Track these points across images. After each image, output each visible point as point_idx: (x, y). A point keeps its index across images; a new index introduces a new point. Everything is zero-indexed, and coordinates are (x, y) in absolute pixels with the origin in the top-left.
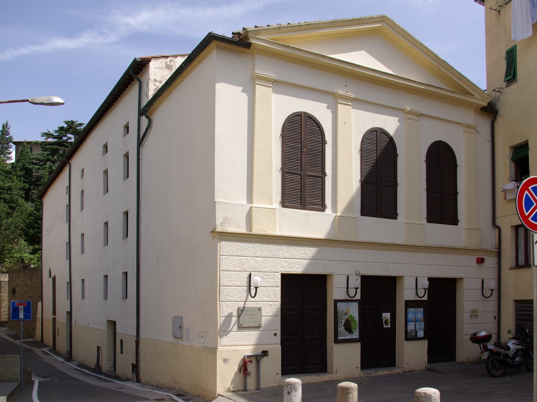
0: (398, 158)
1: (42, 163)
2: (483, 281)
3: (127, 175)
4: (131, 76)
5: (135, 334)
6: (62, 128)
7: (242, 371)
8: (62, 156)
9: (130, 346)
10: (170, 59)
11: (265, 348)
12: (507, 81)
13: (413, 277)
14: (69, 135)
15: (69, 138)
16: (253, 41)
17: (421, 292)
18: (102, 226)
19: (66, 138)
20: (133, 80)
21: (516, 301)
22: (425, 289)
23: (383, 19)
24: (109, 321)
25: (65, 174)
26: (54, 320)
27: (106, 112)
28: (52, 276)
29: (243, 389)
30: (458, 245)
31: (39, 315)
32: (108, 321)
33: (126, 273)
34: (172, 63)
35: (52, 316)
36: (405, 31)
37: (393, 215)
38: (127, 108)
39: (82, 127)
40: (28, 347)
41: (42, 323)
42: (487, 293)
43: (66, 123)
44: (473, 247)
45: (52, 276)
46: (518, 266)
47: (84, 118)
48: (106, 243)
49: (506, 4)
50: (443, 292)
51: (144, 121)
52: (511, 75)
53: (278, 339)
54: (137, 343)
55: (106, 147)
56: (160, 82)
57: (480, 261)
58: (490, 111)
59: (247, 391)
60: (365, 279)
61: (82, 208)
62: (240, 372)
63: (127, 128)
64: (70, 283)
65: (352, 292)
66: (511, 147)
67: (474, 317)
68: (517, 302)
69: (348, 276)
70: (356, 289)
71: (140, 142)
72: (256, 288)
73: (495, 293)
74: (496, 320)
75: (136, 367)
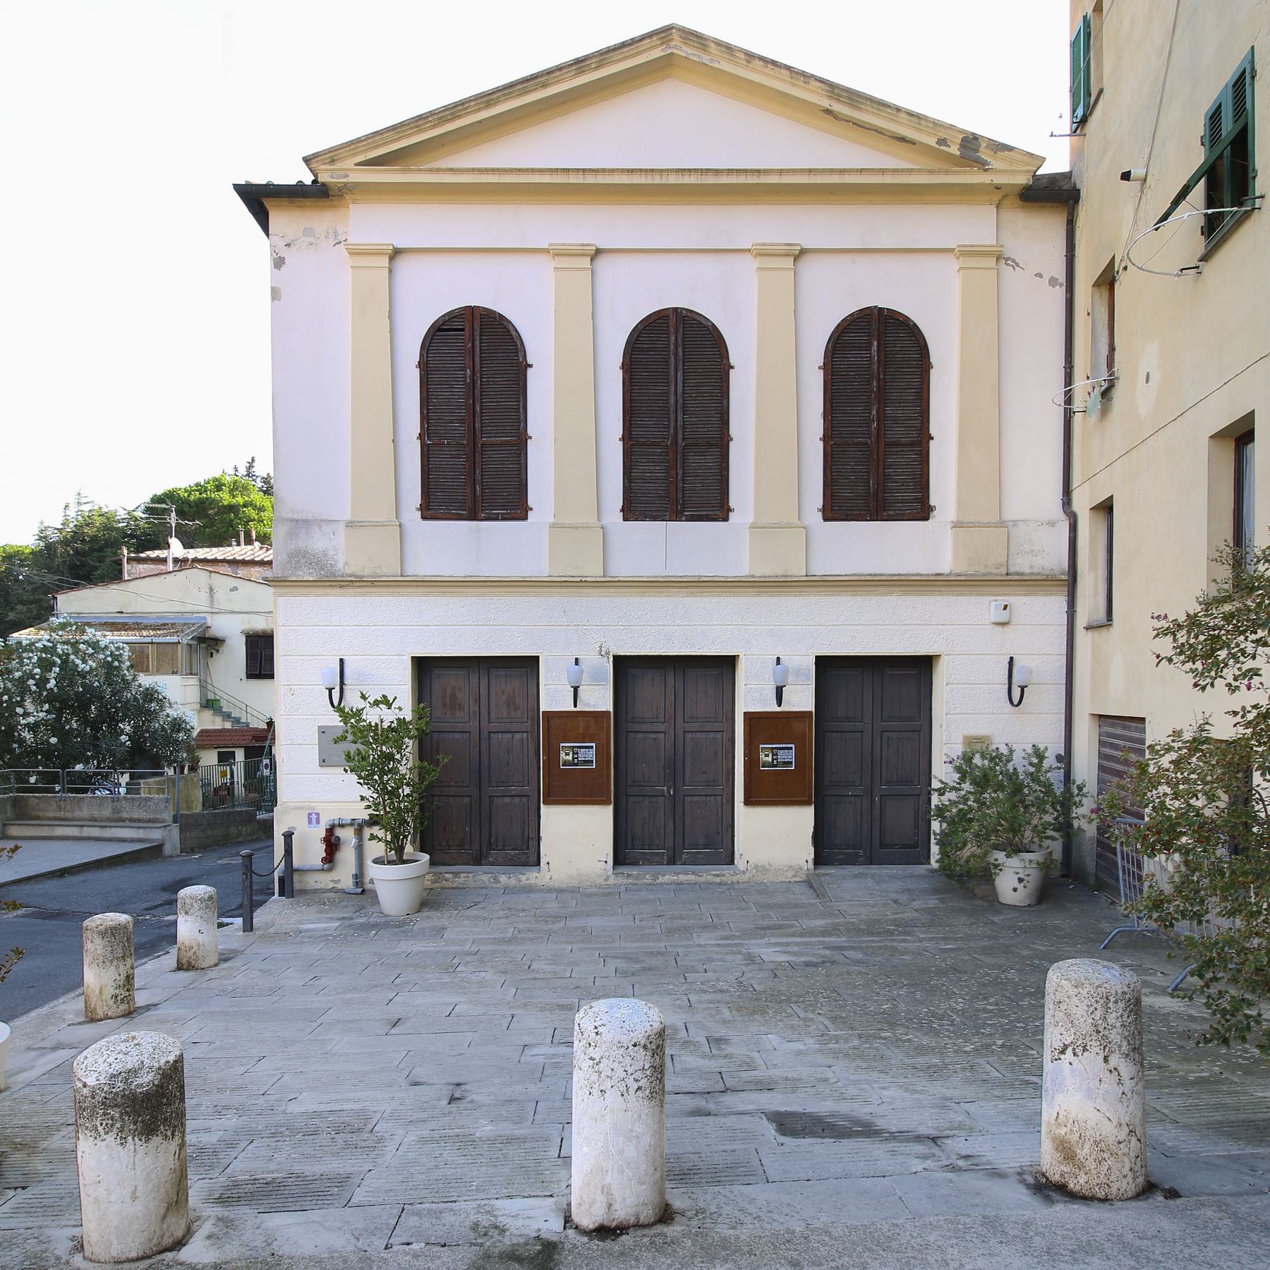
23: (664, 34)
72: (1022, 688)
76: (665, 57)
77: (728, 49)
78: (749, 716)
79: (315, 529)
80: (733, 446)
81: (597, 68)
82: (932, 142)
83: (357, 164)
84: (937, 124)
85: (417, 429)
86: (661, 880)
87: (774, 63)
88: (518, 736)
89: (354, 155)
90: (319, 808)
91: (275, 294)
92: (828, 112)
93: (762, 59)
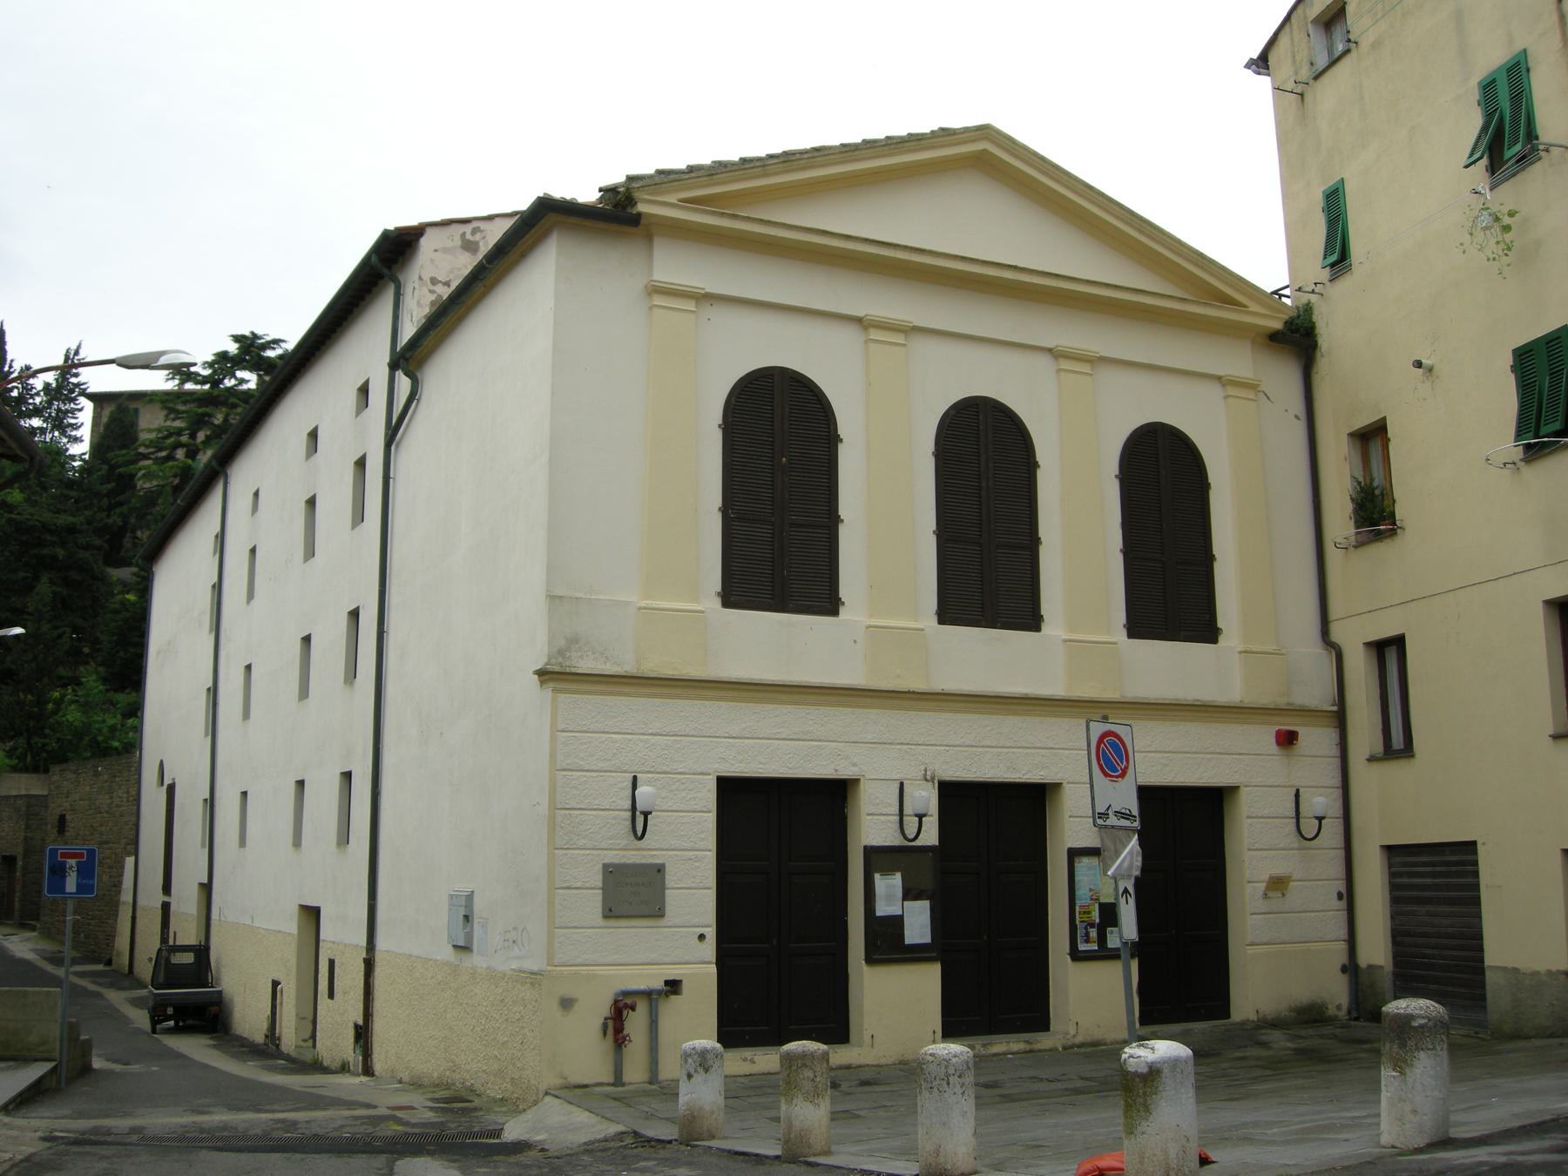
0: (1040, 473)
1: (164, 454)
3: (359, 516)
5: (363, 942)
6: (223, 356)
7: (610, 1031)
8: (218, 432)
9: (350, 978)
10: (475, 224)
11: (673, 972)
12: (1333, 265)
13: (894, 786)
14: (239, 374)
15: (242, 381)
16: (642, 208)
18: (297, 646)
19: (233, 382)
25: (213, 504)
26: (166, 907)
27: (357, 305)
28: (167, 781)
29: (611, 1080)
30: (1221, 699)
31: (126, 896)
34: (478, 237)
35: (162, 898)
36: (1043, 159)
37: (1031, 620)
38: (367, 350)
39: (279, 352)
40: (92, 987)
41: (134, 918)
43: (237, 339)
44: (1264, 700)
45: (167, 781)
47: (288, 328)
48: (304, 693)
49: (1316, 78)
50: (1185, 828)
51: (404, 383)
52: (1339, 255)
53: (709, 950)
54: (369, 965)
55: (313, 435)
56: (447, 284)
57: (1287, 739)
58: (1297, 338)
59: (623, 1085)
60: (951, 792)
61: (251, 595)
62: (605, 1034)
63: (364, 390)
64: (211, 803)
65: (911, 825)
69: (902, 784)
72: (646, 814)
74: (1343, 904)
75: (363, 1034)
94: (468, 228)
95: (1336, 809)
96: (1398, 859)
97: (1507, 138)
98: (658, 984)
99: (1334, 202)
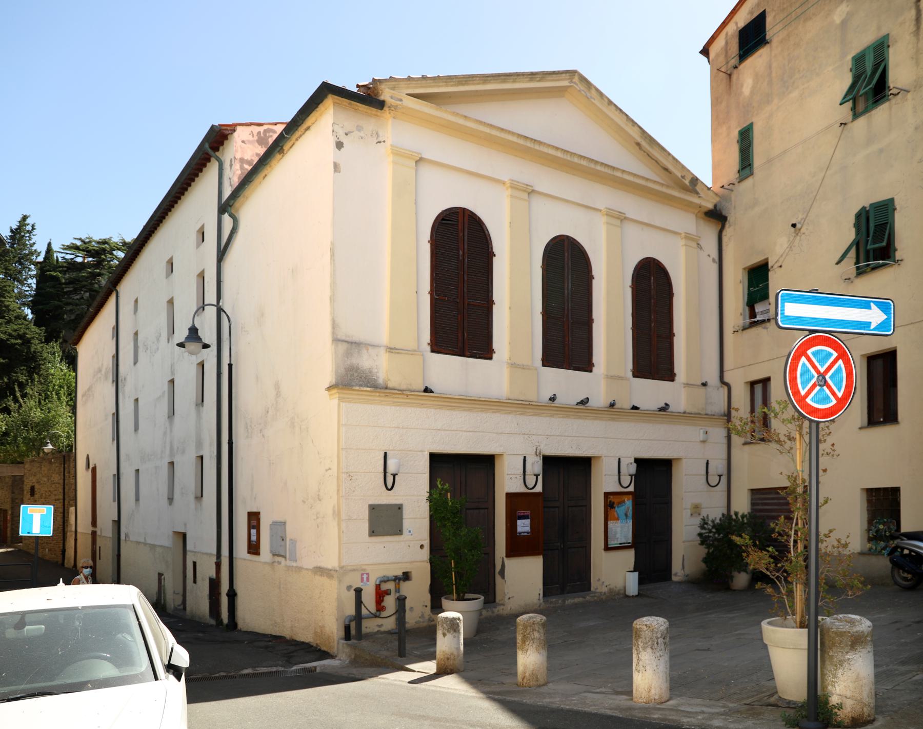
2: (707, 463)
4: (207, 154)
5: (215, 552)
10: (265, 127)
13: (613, 453)
17: (626, 480)
20: (209, 160)
21: (752, 490)
22: (631, 476)
23: (573, 73)
24: (176, 533)
26: (94, 534)
28: (91, 466)
32: (175, 533)
33: (202, 457)
41: (76, 540)
42: (713, 480)
45: (91, 466)
46: (766, 381)
50: (654, 474)
52: (746, 164)
53: (425, 554)
55: (171, 264)
65: (531, 481)
66: (744, 269)
67: (693, 504)
68: (753, 491)
70: (537, 476)
71: (222, 253)
72: (394, 475)
73: (724, 479)
76: (567, 85)
77: (601, 94)
78: (509, 496)
79: (364, 351)
80: (495, 308)
81: (539, 81)
82: (679, 175)
83: (408, 95)
84: (683, 167)
85: (541, 310)
86: (567, 602)
87: (621, 110)
88: (482, 511)
89: (408, 88)
90: (369, 569)
91: (336, 167)
92: (638, 144)
93: (615, 105)
94: (261, 129)
95: (725, 472)
96: (758, 496)
97: (871, 85)
98: (399, 573)
99: (746, 138)
